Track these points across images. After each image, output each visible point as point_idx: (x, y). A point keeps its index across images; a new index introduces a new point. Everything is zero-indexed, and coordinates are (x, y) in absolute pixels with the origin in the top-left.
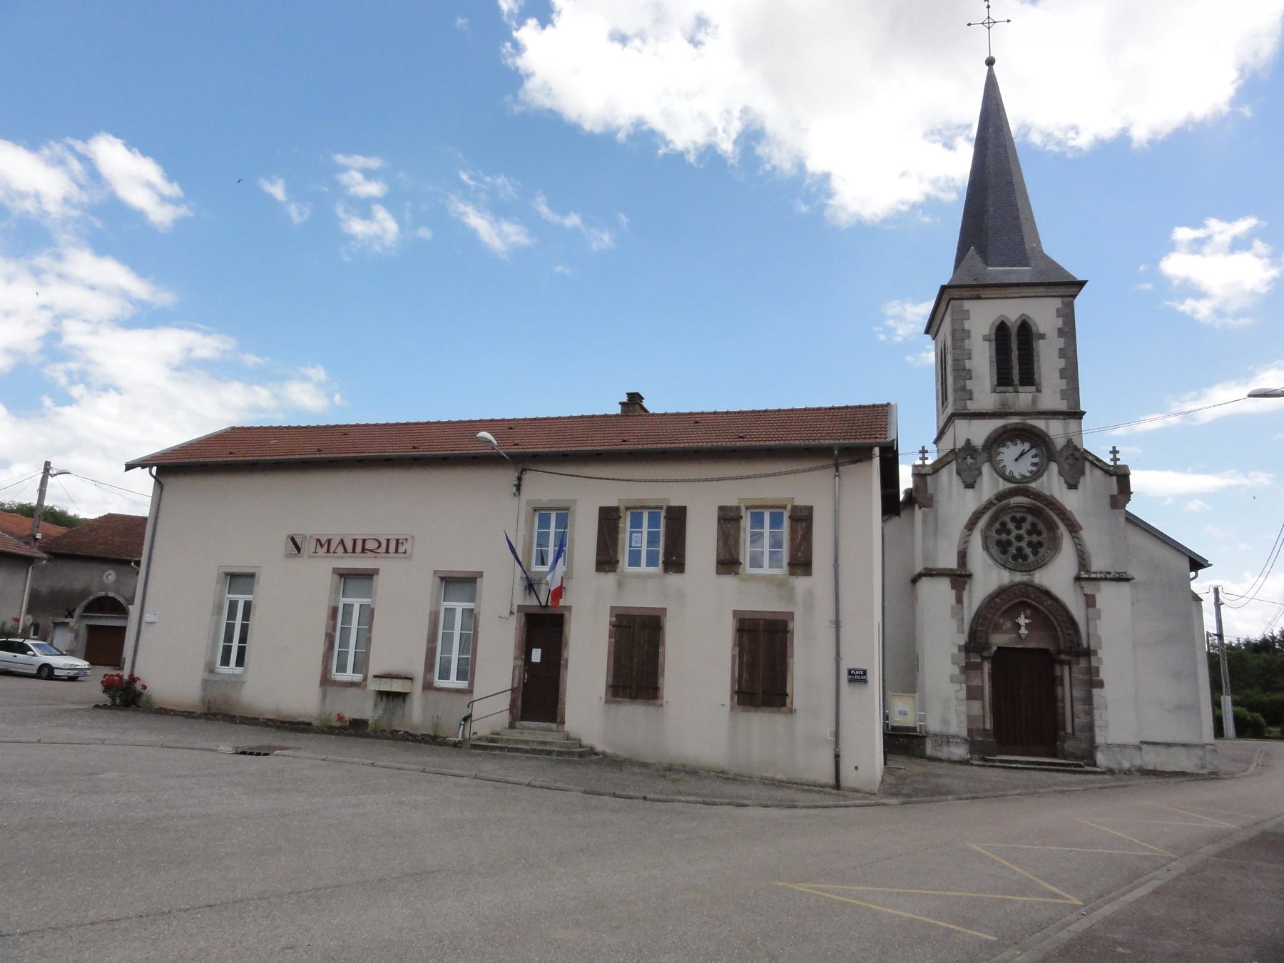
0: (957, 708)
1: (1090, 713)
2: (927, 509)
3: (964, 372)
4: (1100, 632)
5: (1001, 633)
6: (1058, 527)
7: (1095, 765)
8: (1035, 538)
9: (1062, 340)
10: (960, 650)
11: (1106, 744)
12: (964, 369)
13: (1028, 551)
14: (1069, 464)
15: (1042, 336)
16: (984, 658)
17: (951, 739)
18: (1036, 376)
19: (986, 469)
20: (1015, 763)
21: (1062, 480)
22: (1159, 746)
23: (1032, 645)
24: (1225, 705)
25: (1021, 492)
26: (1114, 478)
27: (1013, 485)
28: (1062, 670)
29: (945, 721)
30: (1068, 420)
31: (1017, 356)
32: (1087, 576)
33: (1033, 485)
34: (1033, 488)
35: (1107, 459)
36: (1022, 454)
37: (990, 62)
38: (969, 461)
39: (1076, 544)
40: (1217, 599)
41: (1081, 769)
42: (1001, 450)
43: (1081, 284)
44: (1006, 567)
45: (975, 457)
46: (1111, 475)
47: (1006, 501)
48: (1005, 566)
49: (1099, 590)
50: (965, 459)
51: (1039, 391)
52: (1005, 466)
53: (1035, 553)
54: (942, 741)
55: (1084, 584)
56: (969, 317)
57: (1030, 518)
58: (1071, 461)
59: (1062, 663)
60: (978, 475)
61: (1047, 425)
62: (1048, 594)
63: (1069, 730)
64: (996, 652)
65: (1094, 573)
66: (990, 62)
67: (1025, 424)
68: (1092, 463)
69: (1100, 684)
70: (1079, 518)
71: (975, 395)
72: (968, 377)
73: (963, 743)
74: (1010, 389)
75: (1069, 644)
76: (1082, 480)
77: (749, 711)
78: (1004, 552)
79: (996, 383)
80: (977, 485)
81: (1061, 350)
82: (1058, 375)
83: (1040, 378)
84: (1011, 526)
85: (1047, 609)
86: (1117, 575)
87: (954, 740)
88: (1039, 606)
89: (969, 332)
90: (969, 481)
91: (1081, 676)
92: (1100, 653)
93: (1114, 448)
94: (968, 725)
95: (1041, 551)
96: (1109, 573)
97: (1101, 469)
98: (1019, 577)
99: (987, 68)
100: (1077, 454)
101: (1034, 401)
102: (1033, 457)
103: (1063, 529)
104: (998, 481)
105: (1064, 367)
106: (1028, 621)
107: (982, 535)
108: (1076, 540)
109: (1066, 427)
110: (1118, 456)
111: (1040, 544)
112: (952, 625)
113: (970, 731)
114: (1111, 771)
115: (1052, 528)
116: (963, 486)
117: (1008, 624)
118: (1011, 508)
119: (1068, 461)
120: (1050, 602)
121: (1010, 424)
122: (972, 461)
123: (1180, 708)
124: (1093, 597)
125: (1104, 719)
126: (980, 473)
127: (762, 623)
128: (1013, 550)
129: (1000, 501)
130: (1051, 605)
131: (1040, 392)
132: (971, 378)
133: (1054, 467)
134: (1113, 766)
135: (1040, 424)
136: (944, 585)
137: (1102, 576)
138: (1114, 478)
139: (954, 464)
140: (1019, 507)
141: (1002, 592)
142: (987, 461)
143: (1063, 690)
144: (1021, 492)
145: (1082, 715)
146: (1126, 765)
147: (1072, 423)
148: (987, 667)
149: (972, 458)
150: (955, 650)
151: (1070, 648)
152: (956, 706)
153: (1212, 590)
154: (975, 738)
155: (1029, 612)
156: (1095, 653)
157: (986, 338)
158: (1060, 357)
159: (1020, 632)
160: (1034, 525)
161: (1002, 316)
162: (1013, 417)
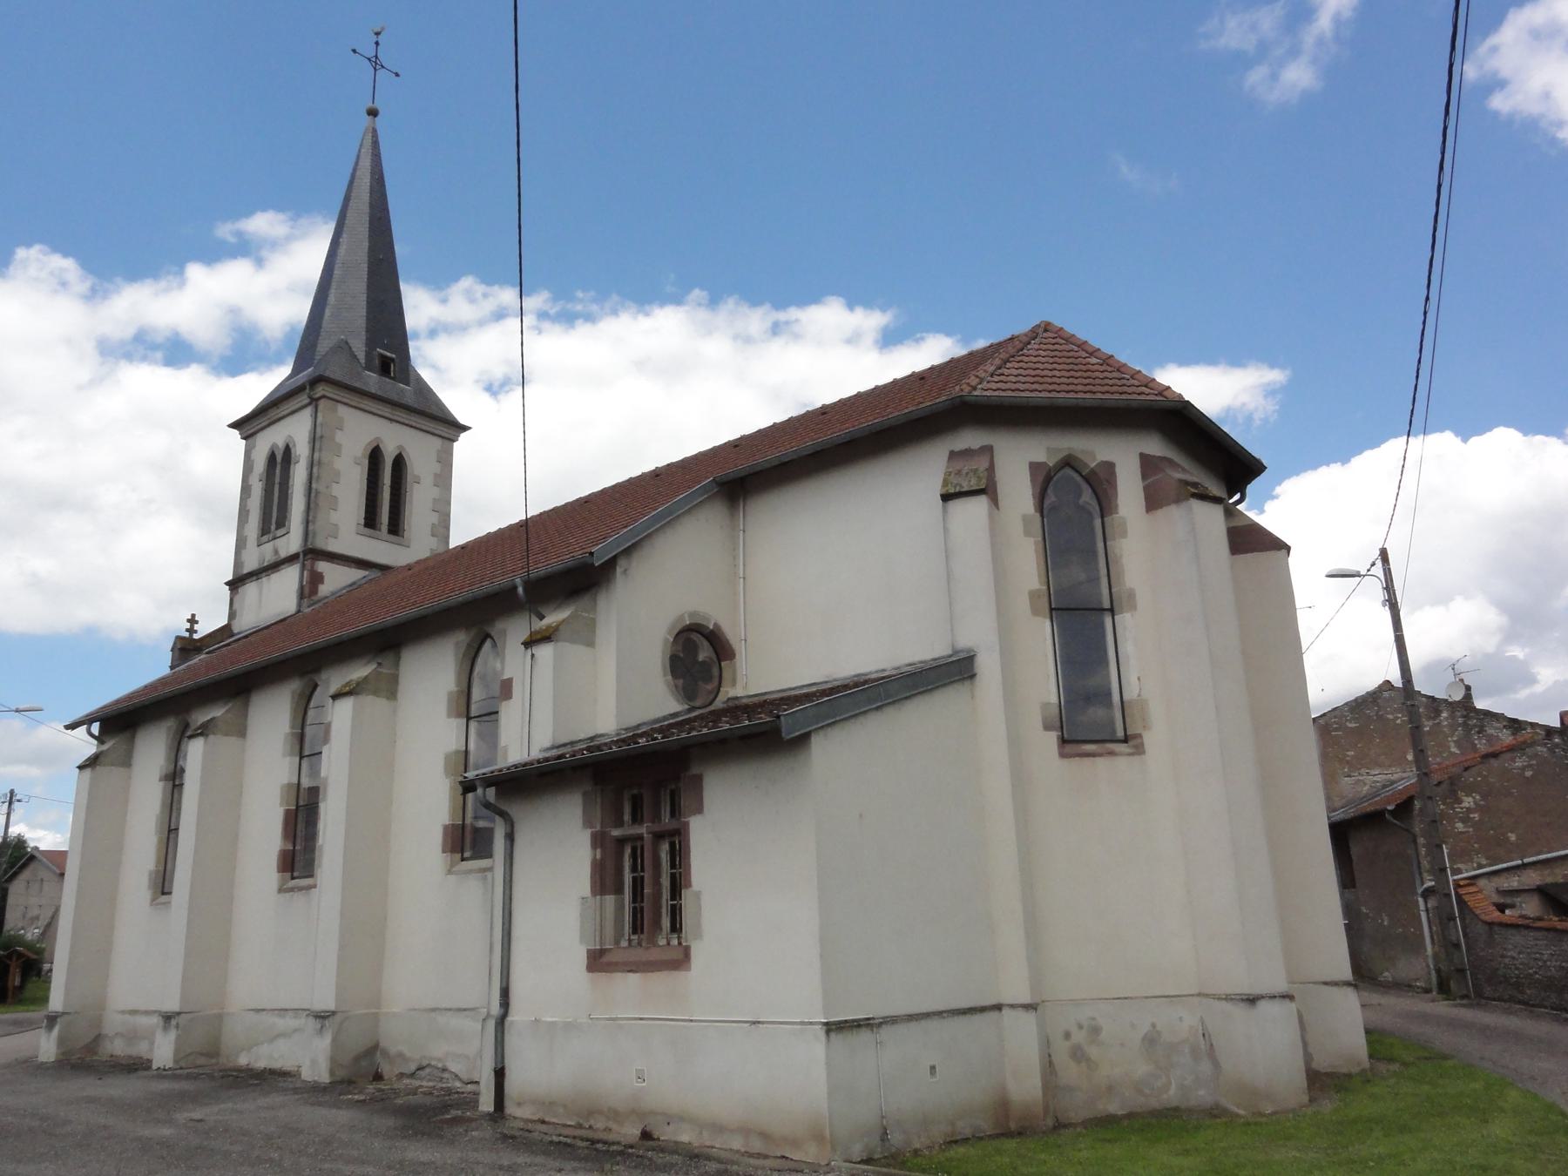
43: (465, 428)
77: (1034, 498)
81: (436, 475)
93: (193, 616)
110: (196, 627)
116: (430, 533)
127: (686, 615)
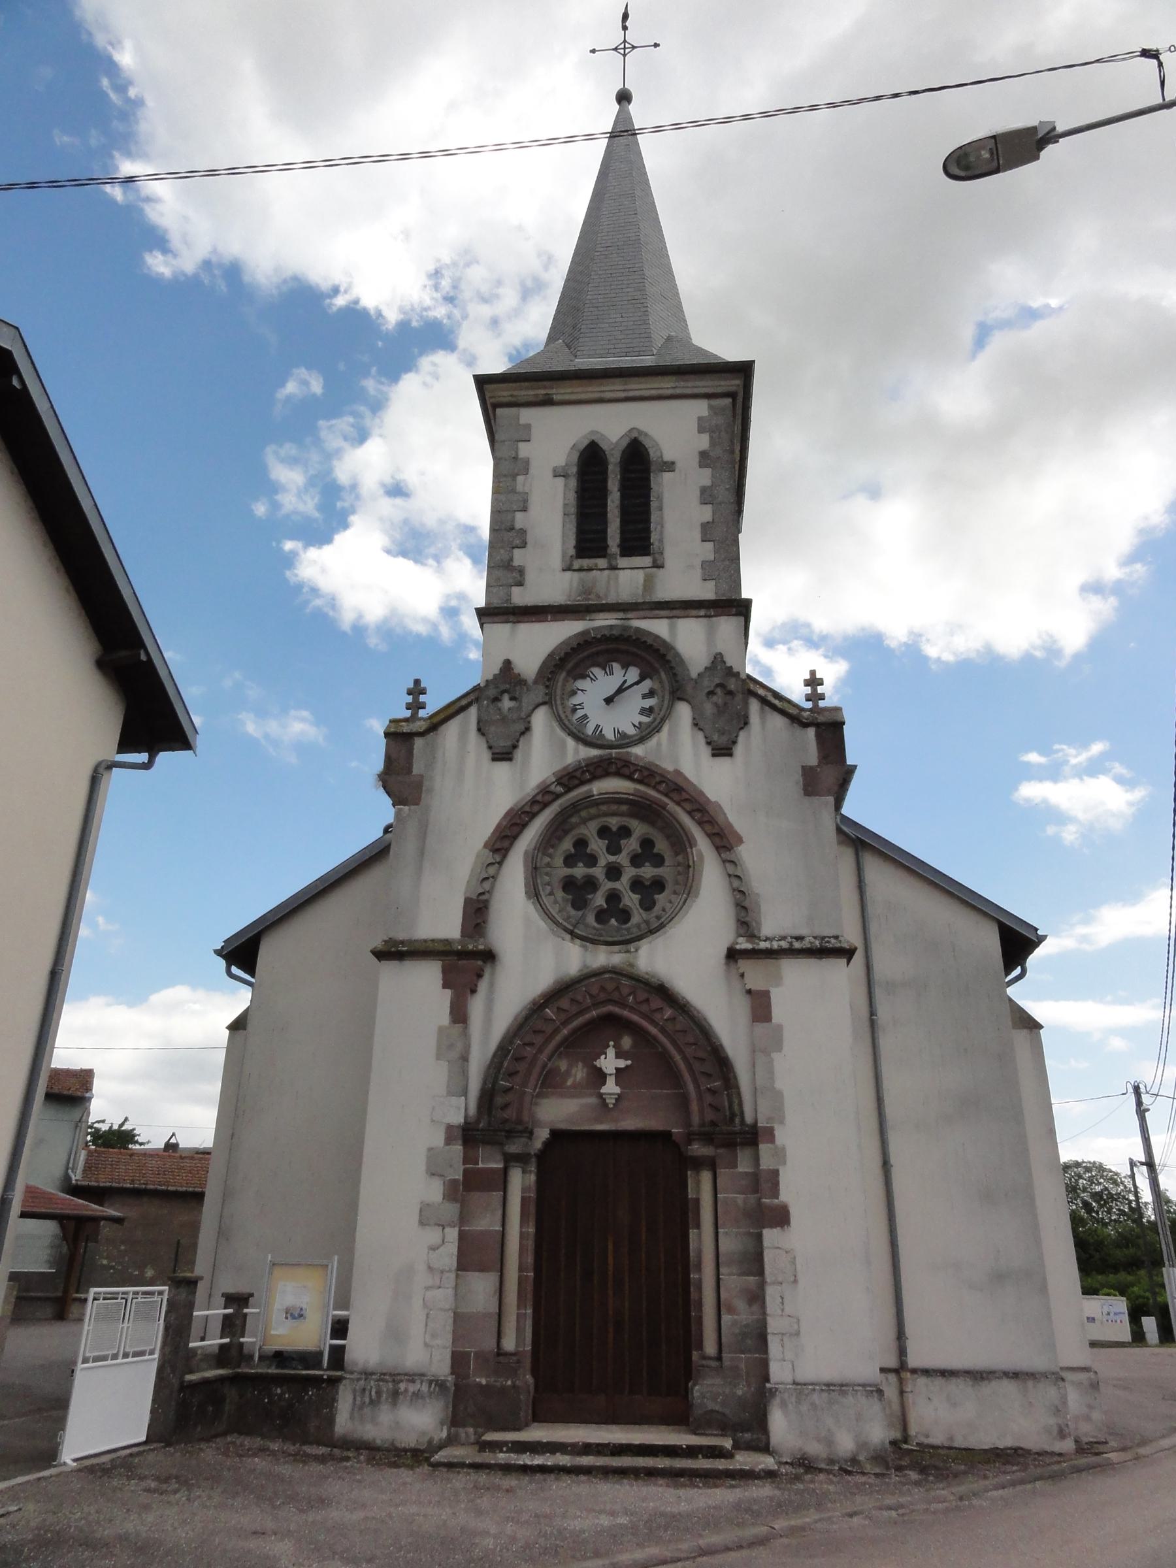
0: (429, 1294)
1: (757, 1298)
2: (406, 808)
3: (512, 534)
4: (782, 1083)
5: (562, 1096)
6: (692, 843)
7: (765, 1448)
8: (648, 872)
9: (707, 472)
10: (449, 1140)
11: (795, 1383)
12: (512, 529)
13: (631, 900)
14: (716, 704)
15: (670, 466)
16: (510, 1159)
17: (402, 1386)
18: (654, 538)
19: (541, 720)
20: (553, 1452)
21: (702, 740)
22: (954, 1380)
23: (630, 1123)
24: (1170, 1283)
25: (613, 769)
26: (811, 732)
27: (594, 752)
28: (698, 1183)
29: (395, 1334)
30: (714, 619)
31: (618, 502)
32: (749, 946)
33: (638, 751)
34: (637, 756)
35: (796, 692)
36: (620, 690)
37: (624, 97)
38: (506, 703)
39: (730, 876)
40: (1139, 1103)
41: (720, 1464)
42: (581, 684)
44: (573, 935)
45: (517, 695)
46: (805, 725)
47: (583, 789)
48: (571, 933)
49: (778, 980)
50: (496, 699)
51: (658, 565)
52: (585, 717)
53: (648, 905)
54: (379, 1393)
55: (744, 965)
56: (530, 437)
57: (639, 829)
58: (719, 698)
59: (698, 1164)
60: (523, 733)
61: (672, 629)
62: (663, 992)
63: (710, 1348)
64: (547, 1144)
65: (767, 939)
66: (624, 97)
67: (626, 628)
68: (764, 701)
69: (781, 1218)
70: (736, 818)
71: (530, 577)
72: (517, 542)
73: (430, 1394)
74: (602, 562)
75: (710, 1115)
76: (742, 735)
78: (579, 904)
79: (572, 552)
80: (518, 754)
81: (703, 490)
82: (697, 534)
83: (661, 541)
84: (597, 846)
85: (663, 1030)
86: (817, 943)
87: (412, 1388)
88: (645, 1024)
89: (527, 462)
90: (502, 744)
91: (740, 1198)
92: (782, 1136)
94: (455, 1340)
95: (661, 899)
96: (799, 938)
97: (783, 712)
98: (602, 958)
99: (616, 107)
100: (732, 685)
101: (649, 584)
102: (644, 697)
103: (703, 845)
104: (563, 745)
105: (710, 520)
106: (622, 1063)
107: (525, 865)
108: (731, 869)
109: (711, 634)
111: (659, 885)
112: (437, 1075)
113: (458, 1360)
114: (805, 1465)
115: (681, 843)
117: (579, 1073)
118: (597, 803)
119: (715, 698)
120: (668, 1013)
121: (595, 629)
122: (512, 704)
123: (999, 1277)
124: (765, 995)
125: (788, 1309)
126: (527, 729)
128: (599, 900)
129: (569, 789)
130: (672, 1019)
131: (662, 567)
132: (523, 545)
133: (684, 712)
134: (814, 1449)
135: (658, 627)
136: (428, 975)
137: (784, 944)
138: (811, 732)
139: (473, 711)
140: (614, 800)
141: (561, 991)
142: (544, 703)
143: (700, 1236)
144: (613, 769)
145: (741, 1305)
146: (846, 1444)
147: (727, 625)
148: (520, 1182)
149: (512, 699)
150: (439, 1140)
151: (713, 1124)
152: (427, 1288)
153: (1131, 1090)
154: (472, 1379)
155: (627, 1042)
156: (770, 1134)
157: (766, 695)
158: (704, 503)
159: (604, 1090)
160: (647, 843)
161: (593, 432)
162: (602, 615)
